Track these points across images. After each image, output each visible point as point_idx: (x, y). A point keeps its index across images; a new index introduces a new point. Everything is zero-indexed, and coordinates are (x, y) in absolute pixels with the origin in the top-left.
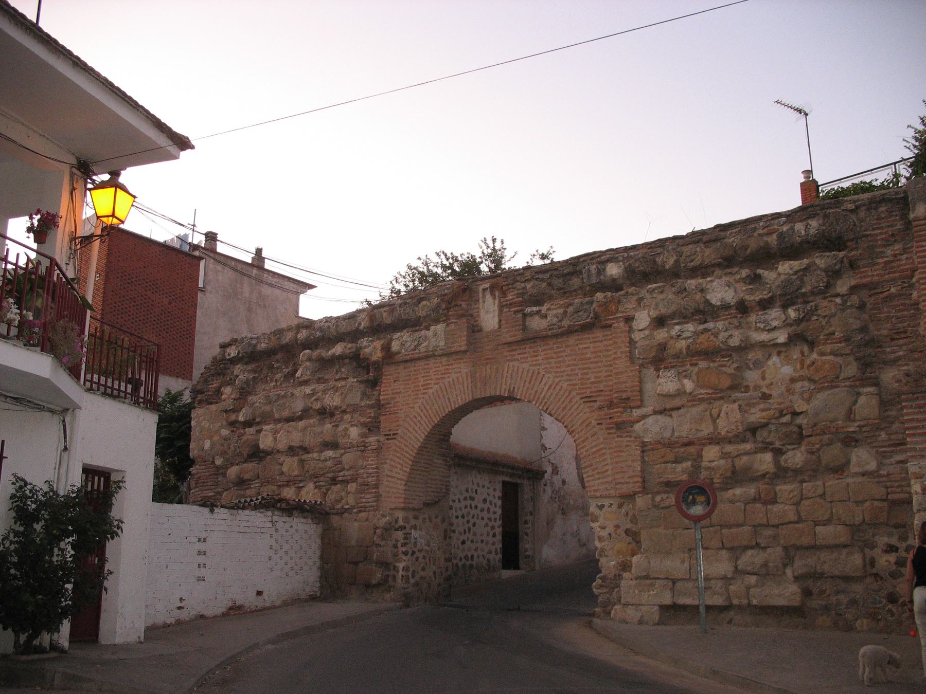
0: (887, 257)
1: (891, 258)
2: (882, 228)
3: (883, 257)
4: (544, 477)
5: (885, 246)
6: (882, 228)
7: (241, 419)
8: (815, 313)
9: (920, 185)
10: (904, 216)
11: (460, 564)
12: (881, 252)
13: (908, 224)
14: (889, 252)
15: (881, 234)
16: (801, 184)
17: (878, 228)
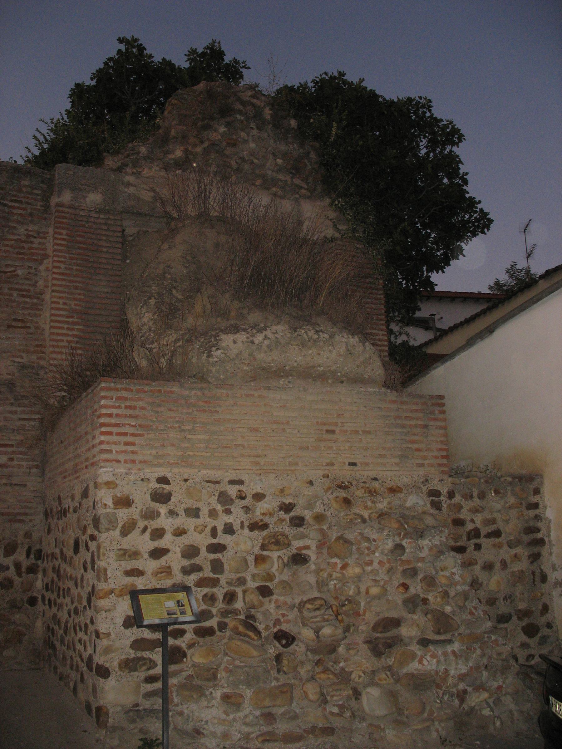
0: (19, 235)
1: (23, 238)
2: (21, 202)
3: (14, 234)
4: (189, 575)
5: (18, 222)
6: (21, 202)
7: (91, 260)
8: (337, 235)
9: (70, 173)
10: (46, 199)
11: (486, 639)
12: (14, 228)
13: (47, 208)
14: (22, 230)
15: (19, 208)
16: (77, 85)
17: (15, 201)
